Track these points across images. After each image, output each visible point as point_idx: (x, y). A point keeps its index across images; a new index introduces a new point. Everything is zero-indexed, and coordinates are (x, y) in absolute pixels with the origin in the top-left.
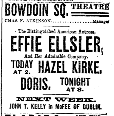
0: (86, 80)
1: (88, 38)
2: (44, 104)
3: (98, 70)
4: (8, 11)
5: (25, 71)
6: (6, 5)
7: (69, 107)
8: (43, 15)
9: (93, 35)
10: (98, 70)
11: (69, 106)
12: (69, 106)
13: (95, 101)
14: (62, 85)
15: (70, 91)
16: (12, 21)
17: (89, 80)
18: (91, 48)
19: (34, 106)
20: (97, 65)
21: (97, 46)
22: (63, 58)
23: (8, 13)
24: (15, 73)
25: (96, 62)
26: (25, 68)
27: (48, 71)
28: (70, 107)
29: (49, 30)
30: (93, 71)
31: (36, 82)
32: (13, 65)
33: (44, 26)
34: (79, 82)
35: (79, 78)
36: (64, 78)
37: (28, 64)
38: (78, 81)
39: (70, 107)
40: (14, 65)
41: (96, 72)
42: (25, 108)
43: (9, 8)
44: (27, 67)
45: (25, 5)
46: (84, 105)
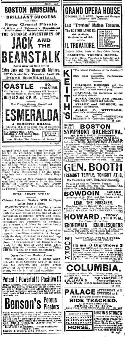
0: (109, 174)
3: (93, 47)
6: (6, 299)
10: (93, 47)
13: (48, 194)
14: (72, 48)
17: (39, 54)
19: (107, 203)
20: (93, 44)
22: (56, 306)
23: (8, 307)
24: (115, 269)
25: (93, 43)
26: (17, 48)
27: (56, 119)
29: (40, 47)
31: (7, 302)
32: (16, 1)
33: (87, 76)
34: (68, 11)
36: (18, 8)
38: (67, 10)
40: (31, 3)
41: (93, 48)
42: (71, 238)
45: (80, 192)
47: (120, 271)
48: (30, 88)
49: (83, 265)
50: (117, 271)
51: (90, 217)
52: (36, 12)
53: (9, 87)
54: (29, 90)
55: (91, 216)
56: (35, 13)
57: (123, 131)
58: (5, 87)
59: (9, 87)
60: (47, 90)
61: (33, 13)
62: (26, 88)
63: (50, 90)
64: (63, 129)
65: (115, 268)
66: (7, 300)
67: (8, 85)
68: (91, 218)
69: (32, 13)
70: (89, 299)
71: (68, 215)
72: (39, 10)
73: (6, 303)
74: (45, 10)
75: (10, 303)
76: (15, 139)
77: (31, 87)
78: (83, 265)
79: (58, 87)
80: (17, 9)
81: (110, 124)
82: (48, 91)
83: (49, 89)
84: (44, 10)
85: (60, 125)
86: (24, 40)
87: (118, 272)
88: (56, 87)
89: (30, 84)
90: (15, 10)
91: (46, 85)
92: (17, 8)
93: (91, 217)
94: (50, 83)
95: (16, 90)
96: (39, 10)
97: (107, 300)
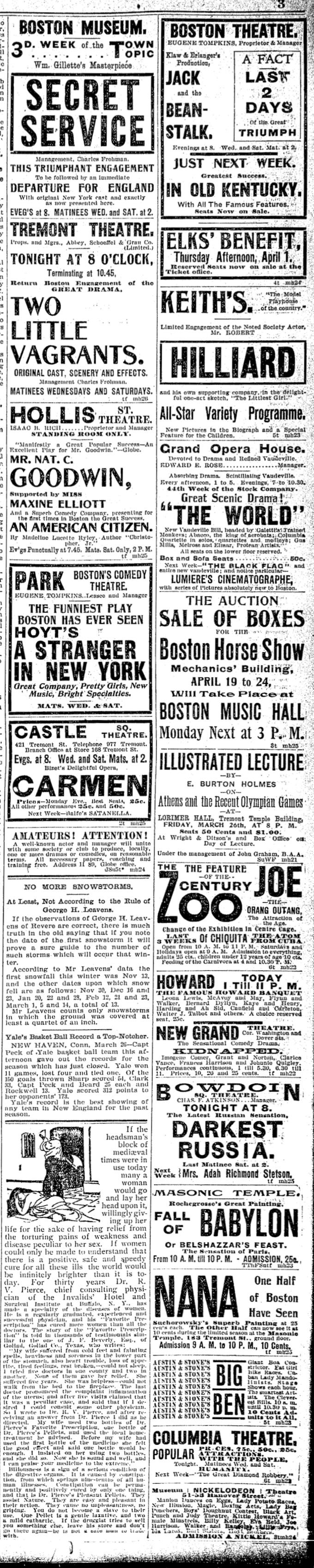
1: (257, 755)
2: (179, 625)
4: (207, 1226)
5: (264, 90)
7: (207, 519)
8: (180, 1433)
9: (275, 157)
11: (207, 511)
12: (207, 511)
14: (299, 705)
15: (267, 111)
16: (280, 107)
17: (279, 1126)
18: (260, 765)
20: (301, 759)
21: (66, 135)
23: (206, 1230)
28: (208, 515)
30: (175, 309)
31: (206, 1218)
35: (275, 184)
37: (224, 1222)
39: (208, 515)
43: (210, 1219)
44: (220, 1232)
46: (21, 22)
47: (272, 1156)
48: (79, 736)
49: (48, 409)
50: (265, 1157)
51: (208, 1129)
52: (97, 32)
53: (26, 735)
54: (76, 740)
55: (212, 1126)
56: (95, 35)
57: (309, 413)
58: (18, 736)
59: (26, 735)
60: (118, 741)
61: (89, 36)
62: (67, 736)
63: (127, 740)
64: (156, 49)
65: (46, 787)
66: (206, 1215)
67: (30, 781)
68: (211, 1133)
69: (86, 36)
70: (184, 507)
71: (23, 409)
72: (104, 28)
73: (162, 711)
74: (57, 95)
75: (169, 648)
76: (47, 813)
77: (80, 733)
78: (48, 409)
79: (148, 733)
80: (54, 648)
81: (174, 380)
82: (122, 743)
83: (123, 739)
84: (115, 28)
85: (151, 591)
86: (72, 86)
87: (269, 1161)
88: (141, 735)
89: (78, 727)
90: (45, 27)
91: (119, 728)
92: (49, 23)
93: (213, 1129)
94: (130, 725)
95: (43, 740)
96: (104, 28)
97: (235, 1128)
